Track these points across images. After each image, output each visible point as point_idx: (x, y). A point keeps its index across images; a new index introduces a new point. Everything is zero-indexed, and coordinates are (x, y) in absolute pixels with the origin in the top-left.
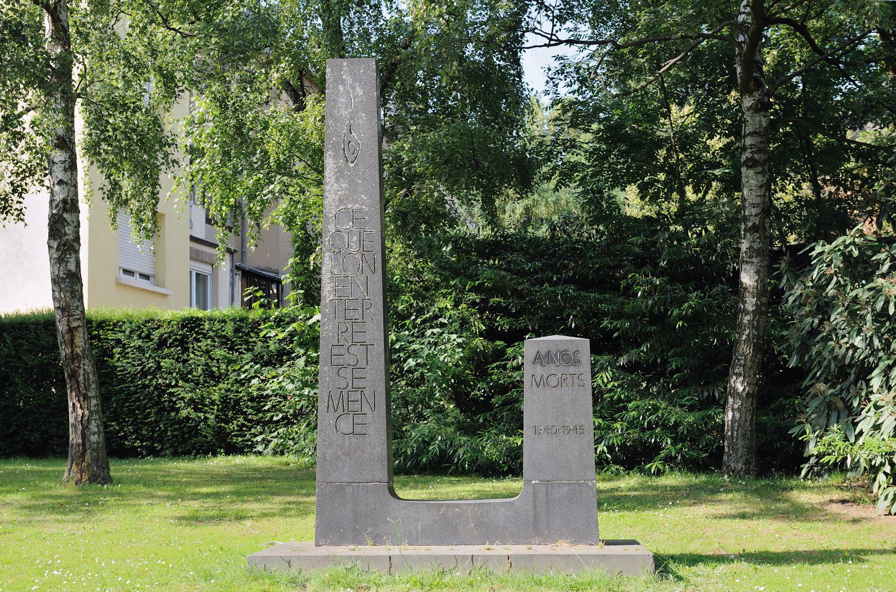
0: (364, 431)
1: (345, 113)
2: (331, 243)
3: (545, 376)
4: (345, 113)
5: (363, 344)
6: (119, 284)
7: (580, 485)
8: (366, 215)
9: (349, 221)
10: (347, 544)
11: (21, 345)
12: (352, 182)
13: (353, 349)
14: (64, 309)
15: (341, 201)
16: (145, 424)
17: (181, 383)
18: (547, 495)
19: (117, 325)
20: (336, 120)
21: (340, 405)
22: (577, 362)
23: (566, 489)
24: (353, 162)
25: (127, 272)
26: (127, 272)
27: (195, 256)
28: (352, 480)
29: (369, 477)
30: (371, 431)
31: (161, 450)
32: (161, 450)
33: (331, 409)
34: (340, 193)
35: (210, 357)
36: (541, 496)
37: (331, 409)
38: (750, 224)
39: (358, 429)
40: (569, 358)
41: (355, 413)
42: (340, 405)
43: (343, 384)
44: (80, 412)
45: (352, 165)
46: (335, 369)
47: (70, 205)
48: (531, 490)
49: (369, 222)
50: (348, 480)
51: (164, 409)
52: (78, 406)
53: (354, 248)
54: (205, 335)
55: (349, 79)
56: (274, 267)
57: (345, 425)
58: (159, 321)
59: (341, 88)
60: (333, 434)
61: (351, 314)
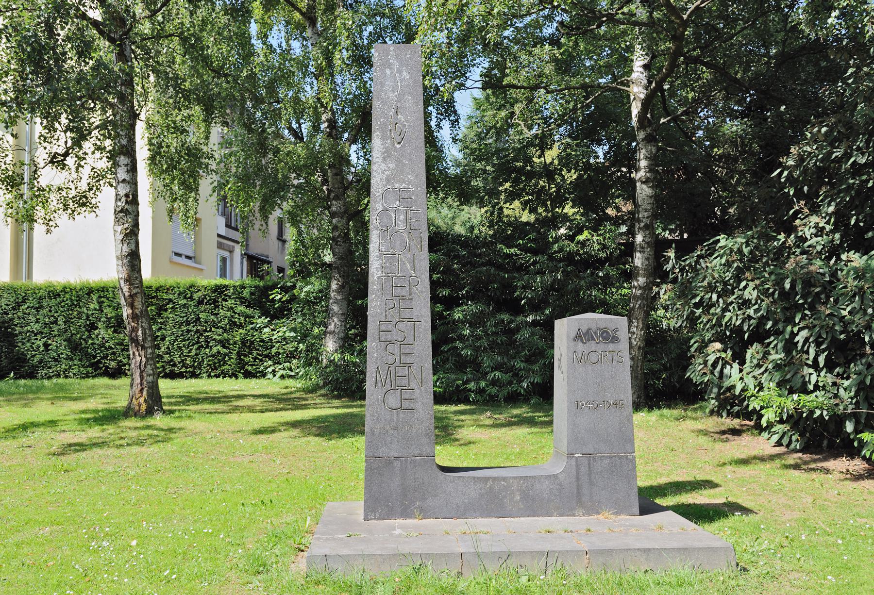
0: (412, 406)
1: (392, 95)
2: (379, 221)
3: (586, 353)
4: (392, 95)
5: (410, 320)
6: (171, 262)
7: (620, 458)
8: (413, 194)
9: (396, 200)
10: (395, 518)
11: (103, 302)
12: (399, 162)
13: (401, 325)
14: (129, 280)
15: (388, 180)
16: (188, 356)
17: (213, 329)
18: (589, 467)
19: (169, 289)
20: (384, 102)
21: (388, 380)
22: (615, 340)
23: (607, 461)
24: (399, 143)
25: (177, 254)
26: (177, 254)
27: (220, 246)
28: (400, 455)
29: (417, 452)
30: (418, 406)
31: (200, 373)
32: (200, 373)
33: (379, 384)
34: (387, 173)
35: (234, 312)
36: (584, 469)
37: (379, 384)
38: (642, 225)
39: (406, 404)
40: (609, 337)
41: (403, 388)
42: (388, 380)
43: (391, 360)
44: (138, 358)
45: (399, 146)
46: (383, 345)
47: (133, 200)
48: (574, 463)
49: (415, 201)
50: (396, 455)
51: (202, 346)
52: (137, 354)
53: (401, 226)
54: (230, 297)
55: (396, 64)
56: (266, 254)
57: (393, 400)
58: (199, 286)
59: (388, 72)
60: (381, 409)
61: (398, 291)
